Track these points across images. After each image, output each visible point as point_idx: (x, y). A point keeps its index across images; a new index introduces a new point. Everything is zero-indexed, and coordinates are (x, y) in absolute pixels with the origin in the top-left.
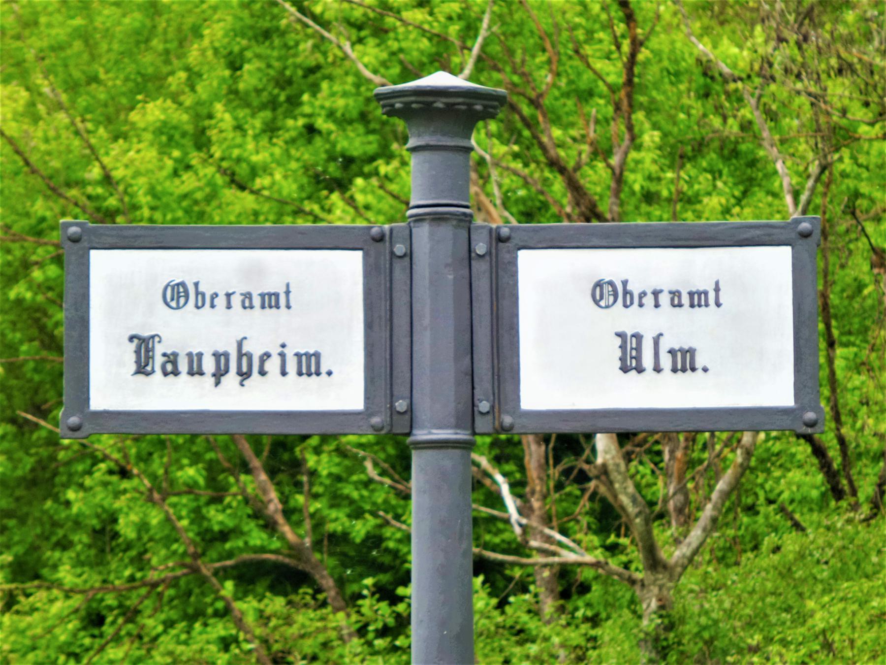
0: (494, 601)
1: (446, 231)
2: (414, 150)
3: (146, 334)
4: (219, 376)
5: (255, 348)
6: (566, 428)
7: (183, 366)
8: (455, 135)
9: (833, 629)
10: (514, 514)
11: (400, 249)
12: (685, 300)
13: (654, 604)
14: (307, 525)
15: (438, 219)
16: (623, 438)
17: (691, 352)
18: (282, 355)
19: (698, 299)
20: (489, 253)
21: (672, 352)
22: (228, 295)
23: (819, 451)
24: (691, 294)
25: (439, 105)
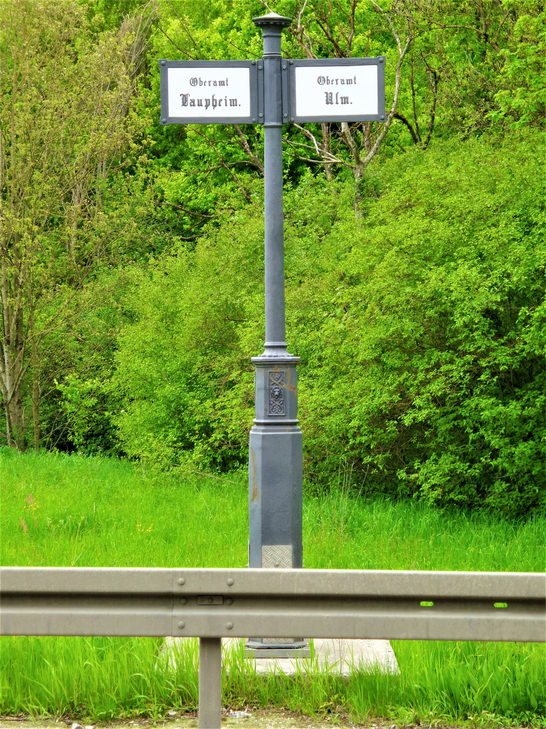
0: (313, 175)
1: (274, 62)
2: (264, 37)
3: (185, 94)
4: (207, 106)
5: (217, 98)
6: (331, 121)
7: (196, 103)
8: (276, 32)
9: (411, 180)
10: (317, 148)
11: (260, 67)
12: (345, 82)
13: (359, 175)
14: (257, 152)
15: (272, 58)
16: (350, 124)
17: (347, 98)
18: (226, 100)
19: (349, 82)
20: (287, 68)
21: (341, 98)
22: (209, 82)
23: (410, 127)
24: (347, 80)
25: (271, 23)
